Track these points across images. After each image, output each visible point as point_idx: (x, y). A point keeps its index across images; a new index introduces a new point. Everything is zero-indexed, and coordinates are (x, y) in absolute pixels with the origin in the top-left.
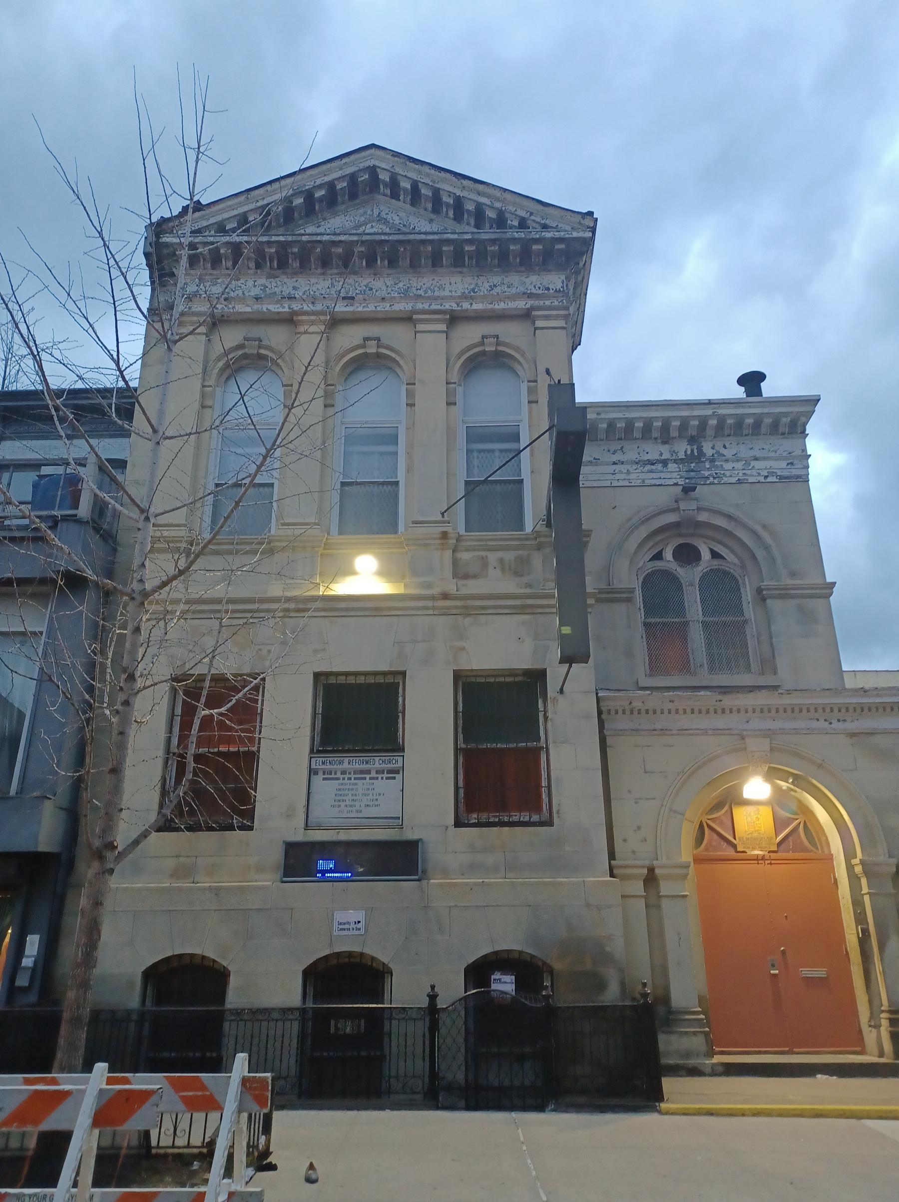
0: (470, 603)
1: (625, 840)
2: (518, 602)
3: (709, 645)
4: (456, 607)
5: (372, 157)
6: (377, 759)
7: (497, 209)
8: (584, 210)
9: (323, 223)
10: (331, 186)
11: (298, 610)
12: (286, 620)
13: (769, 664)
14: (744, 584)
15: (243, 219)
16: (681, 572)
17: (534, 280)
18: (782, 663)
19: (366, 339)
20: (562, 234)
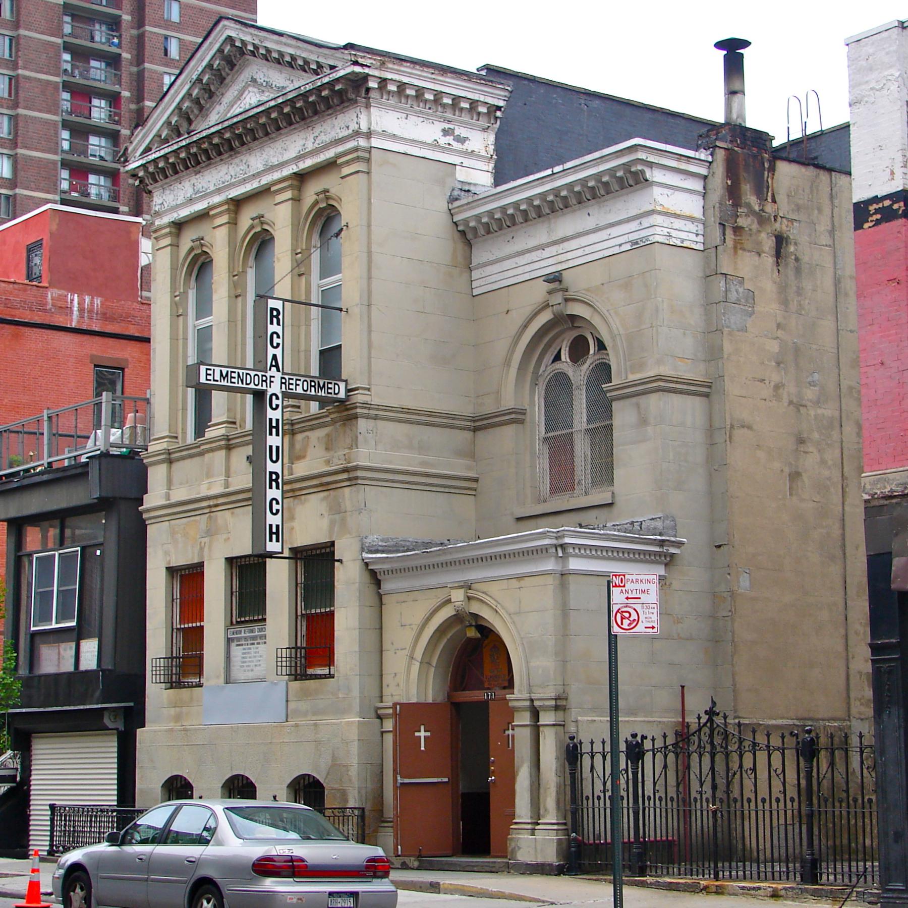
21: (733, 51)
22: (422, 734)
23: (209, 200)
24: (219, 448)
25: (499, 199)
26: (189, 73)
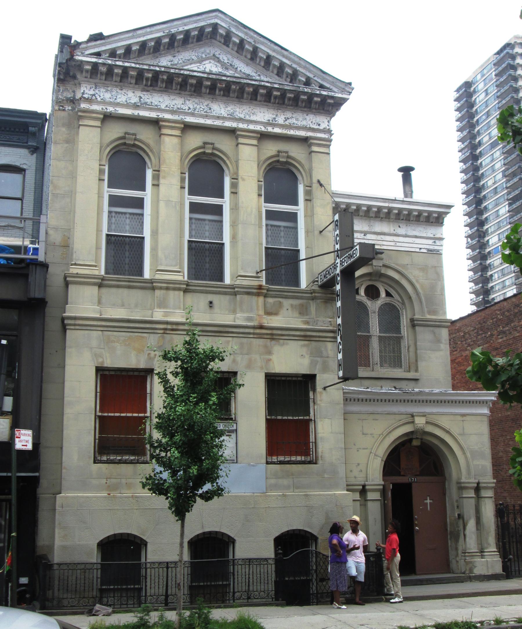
0: (275, 332)
1: (351, 471)
2: (302, 333)
3: (381, 351)
4: (267, 334)
5: (216, 17)
6: (221, 424)
7: (293, 68)
8: (347, 81)
9: (177, 54)
10: (187, 33)
11: (173, 330)
12: (165, 335)
13: (414, 366)
14: (403, 314)
15: (128, 49)
16: (369, 303)
17: (311, 118)
18: (421, 365)
19: (205, 143)
20: (333, 93)
21: (406, 172)
22: (428, 501)
23: (159, 114)
24: (94, 284)
25: (350, 198)
26: (171, 26)
